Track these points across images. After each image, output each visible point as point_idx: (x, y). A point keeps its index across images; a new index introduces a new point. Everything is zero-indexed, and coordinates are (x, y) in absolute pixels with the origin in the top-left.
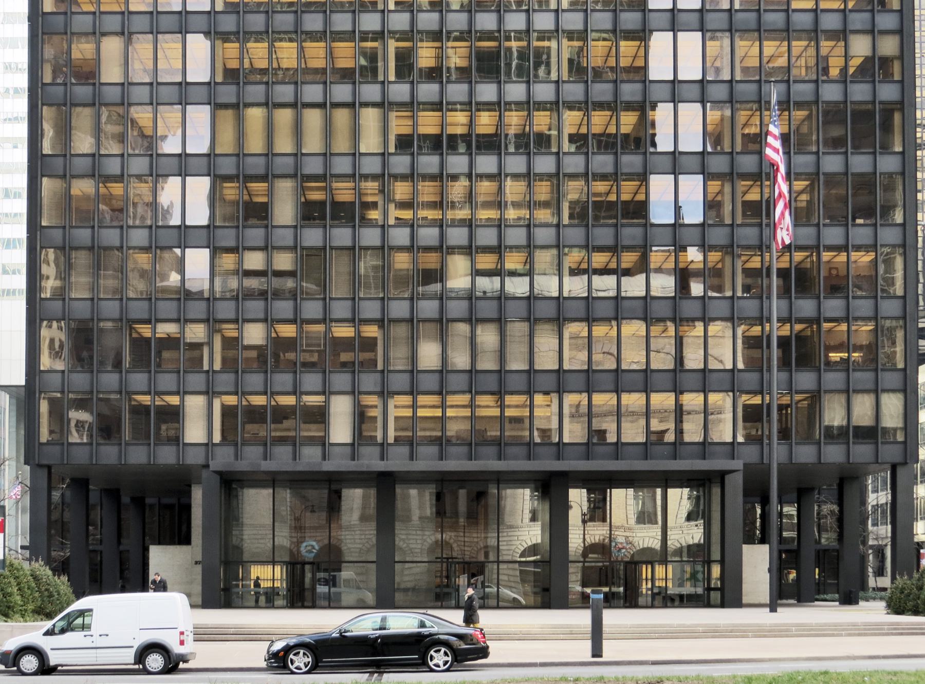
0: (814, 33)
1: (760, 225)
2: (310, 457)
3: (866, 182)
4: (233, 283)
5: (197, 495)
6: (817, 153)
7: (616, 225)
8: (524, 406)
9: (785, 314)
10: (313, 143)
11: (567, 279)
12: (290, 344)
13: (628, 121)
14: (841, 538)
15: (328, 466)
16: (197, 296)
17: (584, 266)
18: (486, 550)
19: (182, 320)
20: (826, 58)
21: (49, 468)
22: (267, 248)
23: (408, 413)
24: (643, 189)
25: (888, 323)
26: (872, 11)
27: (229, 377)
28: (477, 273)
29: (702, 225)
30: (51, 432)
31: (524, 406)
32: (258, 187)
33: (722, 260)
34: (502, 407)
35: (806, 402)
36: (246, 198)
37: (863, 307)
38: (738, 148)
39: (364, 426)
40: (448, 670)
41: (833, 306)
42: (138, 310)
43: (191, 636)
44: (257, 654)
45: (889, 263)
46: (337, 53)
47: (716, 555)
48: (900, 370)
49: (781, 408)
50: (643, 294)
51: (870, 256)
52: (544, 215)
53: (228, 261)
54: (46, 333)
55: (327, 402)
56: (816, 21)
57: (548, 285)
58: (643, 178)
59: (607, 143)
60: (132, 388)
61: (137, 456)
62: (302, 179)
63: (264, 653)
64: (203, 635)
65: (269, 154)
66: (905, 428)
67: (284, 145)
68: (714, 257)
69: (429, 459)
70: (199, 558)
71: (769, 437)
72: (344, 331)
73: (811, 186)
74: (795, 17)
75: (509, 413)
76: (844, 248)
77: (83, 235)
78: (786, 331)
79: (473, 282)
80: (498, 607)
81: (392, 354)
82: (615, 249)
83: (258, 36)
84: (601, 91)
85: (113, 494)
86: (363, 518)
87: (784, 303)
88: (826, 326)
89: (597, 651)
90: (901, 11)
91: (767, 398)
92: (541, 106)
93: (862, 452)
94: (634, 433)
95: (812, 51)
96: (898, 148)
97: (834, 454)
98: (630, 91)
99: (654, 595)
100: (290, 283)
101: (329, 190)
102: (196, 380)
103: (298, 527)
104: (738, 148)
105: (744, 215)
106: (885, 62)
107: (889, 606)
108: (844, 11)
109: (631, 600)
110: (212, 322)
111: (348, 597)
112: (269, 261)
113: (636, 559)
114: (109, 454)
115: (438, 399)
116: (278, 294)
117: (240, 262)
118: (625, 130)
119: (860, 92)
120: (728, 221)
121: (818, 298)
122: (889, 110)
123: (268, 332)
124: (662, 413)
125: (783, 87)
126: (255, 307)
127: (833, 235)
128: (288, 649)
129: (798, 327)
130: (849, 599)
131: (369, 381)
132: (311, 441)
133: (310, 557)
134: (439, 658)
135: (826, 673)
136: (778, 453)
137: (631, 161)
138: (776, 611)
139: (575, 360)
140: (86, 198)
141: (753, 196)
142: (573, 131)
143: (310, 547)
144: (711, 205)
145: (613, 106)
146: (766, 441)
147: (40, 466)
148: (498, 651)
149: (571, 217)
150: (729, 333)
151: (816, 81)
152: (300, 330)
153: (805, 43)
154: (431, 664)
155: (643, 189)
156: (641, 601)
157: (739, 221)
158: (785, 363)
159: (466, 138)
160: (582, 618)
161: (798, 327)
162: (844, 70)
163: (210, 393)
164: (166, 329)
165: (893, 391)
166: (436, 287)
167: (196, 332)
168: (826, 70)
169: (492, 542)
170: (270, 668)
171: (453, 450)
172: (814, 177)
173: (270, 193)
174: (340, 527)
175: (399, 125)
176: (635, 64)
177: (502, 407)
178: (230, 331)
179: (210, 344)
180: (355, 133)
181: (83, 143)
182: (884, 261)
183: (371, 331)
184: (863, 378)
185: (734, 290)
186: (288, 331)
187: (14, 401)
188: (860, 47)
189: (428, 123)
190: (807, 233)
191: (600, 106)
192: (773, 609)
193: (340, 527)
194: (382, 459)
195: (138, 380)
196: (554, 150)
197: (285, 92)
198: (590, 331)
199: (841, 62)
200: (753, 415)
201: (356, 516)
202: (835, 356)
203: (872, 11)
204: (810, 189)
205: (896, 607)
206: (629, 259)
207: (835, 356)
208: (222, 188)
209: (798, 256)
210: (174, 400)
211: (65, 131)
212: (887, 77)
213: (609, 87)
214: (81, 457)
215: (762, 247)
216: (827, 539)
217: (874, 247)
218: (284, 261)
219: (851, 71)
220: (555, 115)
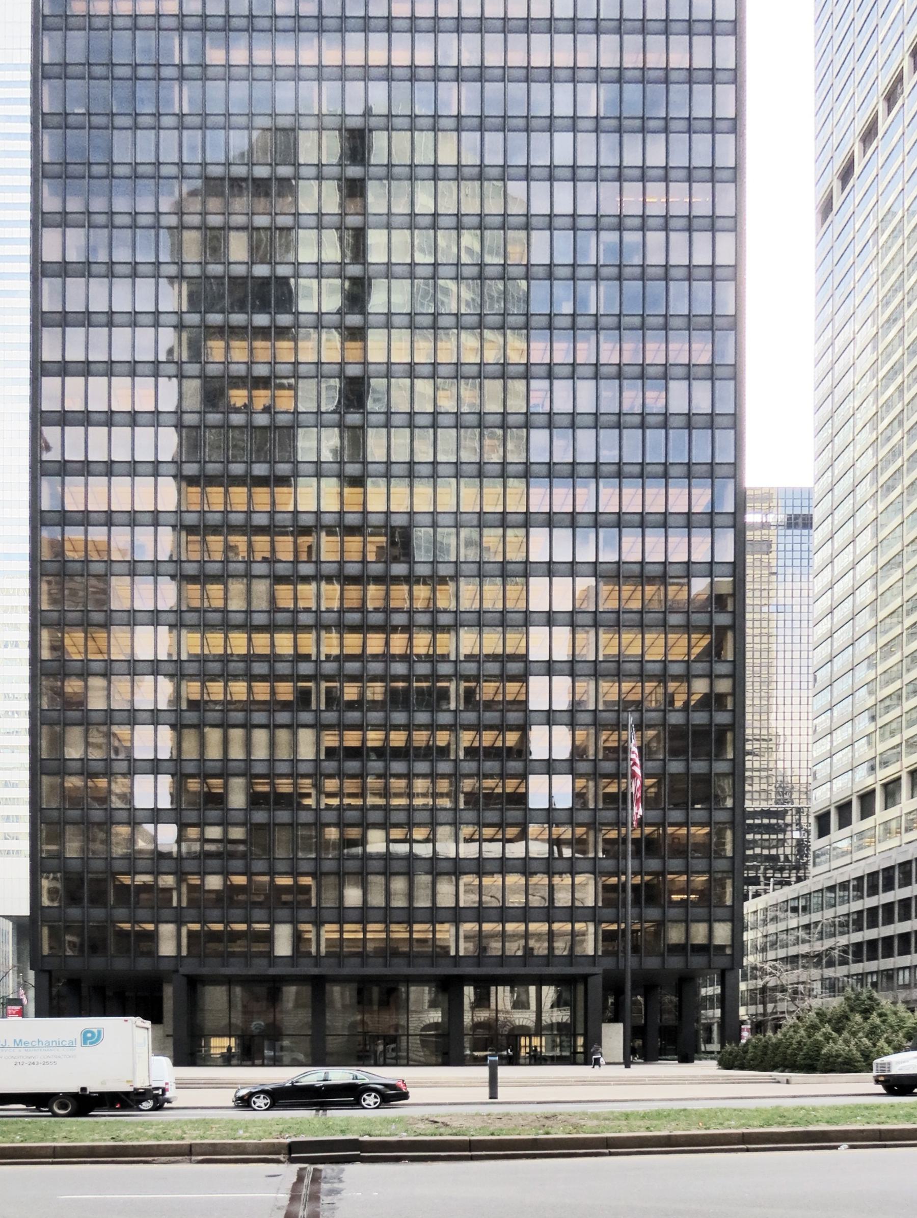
0: (663, 677)
1: (618, 809)
2: (259, 967)
3: (706, 779)
4: (196, 847)
5: (168, 991)
6: (664, 760)
7: (502, 711)
9: (637, 869)
10: (260, 752)
11: (462, 845)
12: (241, 889)
13: (512, 738)
14: (680, 1017)
15: (272, 971)
16: (167, 856)
17: (476, 837)
18: (397, 1027)
19: (156, 873)
20: (672, 695)
21: (50, 972)
22: (225, 823)
23: (336, 936)
24: (523, 785)
25: (719, 876)
26: (711, 662)
27: (193, 912)
28: (389, 841)
29: (571, 809)
30: (51, 948)
32: (216, 782)
33: (587, 833)
34: (365, 931)
36: (206, 789)
37: (700, 864)
38: (601, 756)
39: (301, 945)
40: (377, 1108)
41: (675, 864)
42: (118, 865)
43: (174, 1086)
44: (227, 1097)
45: (721, 834)
46: (255, 690)
47: (580, 1029)
49: (634, 932)
50: (523, 855)
51: (706, 830)
52: (446, 803)
53: (193, 832)
54: (45, 884)
55: (272, 928)
56: (665, 668)
57: (446, 849)
58: (524, 777)
59: (493, 753)
60: (116, 919)
61: (121, 964)
62: (249, 774)
63: (232, 1097)
64: (182, 1085)
65: (225, 760)
66: (732, 946)
67: (283, 753)
68: (580, 831)
69: (352, 968)
71: (624, 952)
72: (284, 881)
73: (659, 783)
74: (649, 666)
75: (415, 936)
76: (686, 824)
77: (74, 814)
78: (637, 880)
79: (388, 847)
80: (408, 1065)
81: (323, 896)
82: (501, 825)
83: (263, 678)
84: (491, 717)
86: (297, 1005)
87: (637, 862)
88: (670, 877)
89: (493, 1095)
90: (734, 661)
92: (443, 727)
93: (697, 961)
94: (515, 948)
95: (661, 690)
96: (730, 756)
97: (675, 963)
98: (514, 717)
99: (531, 1057)
100: (242, 848)
101: (273, 785)
102: (166, 913)
103: (247, 1012)
104: (601, 756)
105: (604, 802)
106: (721, 698)
107: (720, 1064)
108: (687, 661)
109: (513, 1061)
110: (180, 876)
111: (286, 1059)
112: (225, 832)
113: (516, 1032)
114: (98, 963)
115: (355, 737)
116: (232, 855)
117: (202, 833)
118: (508, 744)
119: (699, 718)
120: (591, 805)
121: (663, 858)
122: (722, 730)
123: (225, 881)
124: (539, 936)
125: (637, 715)
126: (214, 863)
127: (676, 815)
128: (251, 1095)
129: (647, 878)
130: (686, 1058)
131: (304, 914)
132: (261, 955)
133: (256, 1032)
134: (370, 1100)
135: (685, 1110)
136: (631, 962)
137: (514, 766)
139: (467, 900)
140: (76, 788)
141: (613, 789)
142: (467, 744)
143: (257, 1024)
144: (578, 796)
145: (502, 728)
146: (621, 954)
148: (415, 1095)
149: (466, 803)
150: (592, 882)
151: (664, 711)
152: (250, 880)
153: (655, 684)
154: (255, 1107)
155: (523, 785)
156: (522, 1061)
157: (601, 806)
158: (637, 902)
159: (428, 749)
160: (483, 1072)
161: (647, 878)
162: (687, 703)
163: (179, 922)
164: (141, 879)
165: (724, 921)
166: (359, 850)
167: (168, 881)
168: (672, 702)
169: (403, 1022)
170: (237, 1107)
171: (371, 960)
172: (661, 777)
173: (226, 786)
174: (281, 1012)
175: (330, 740)
176: (518, 698)
177: (411, 932)
178: (194, 880)
179: (179, 889)
180: (294, 745)
181: (74, 752)
182: (716, 834)
183: (306, 881)
184: (701, 912)
185: (596, 852)
186: (240, 880)
188: (700, 687)
189: (352, 739)
190: (654, 815)
191: (490, 728)
192: (627, 1066)
193: (281, 1012)
194: (316, 966)
195: (121, 912)
196: (452, 757)
197: (238, 717)
198: (480, 882)
199: (685, 697)
200: (609, 937)
201: (338, 1005)
202: (675, 897)
203: (711, 662)
204: (658, 785)
205: (726, 1064)
206: (511, 832)
207: (675, 897)
208: (186, 783)
209: (648, 830)
210: (150, 927)
211: (59, 742)
212: (721, 707)
213: (497, 714)
214: (76, 965)
215: (619, 823)
216: (669, 1019)
217: (708, 824)
218: (237, 833)
219: (692, 703)
220: (453, 735)
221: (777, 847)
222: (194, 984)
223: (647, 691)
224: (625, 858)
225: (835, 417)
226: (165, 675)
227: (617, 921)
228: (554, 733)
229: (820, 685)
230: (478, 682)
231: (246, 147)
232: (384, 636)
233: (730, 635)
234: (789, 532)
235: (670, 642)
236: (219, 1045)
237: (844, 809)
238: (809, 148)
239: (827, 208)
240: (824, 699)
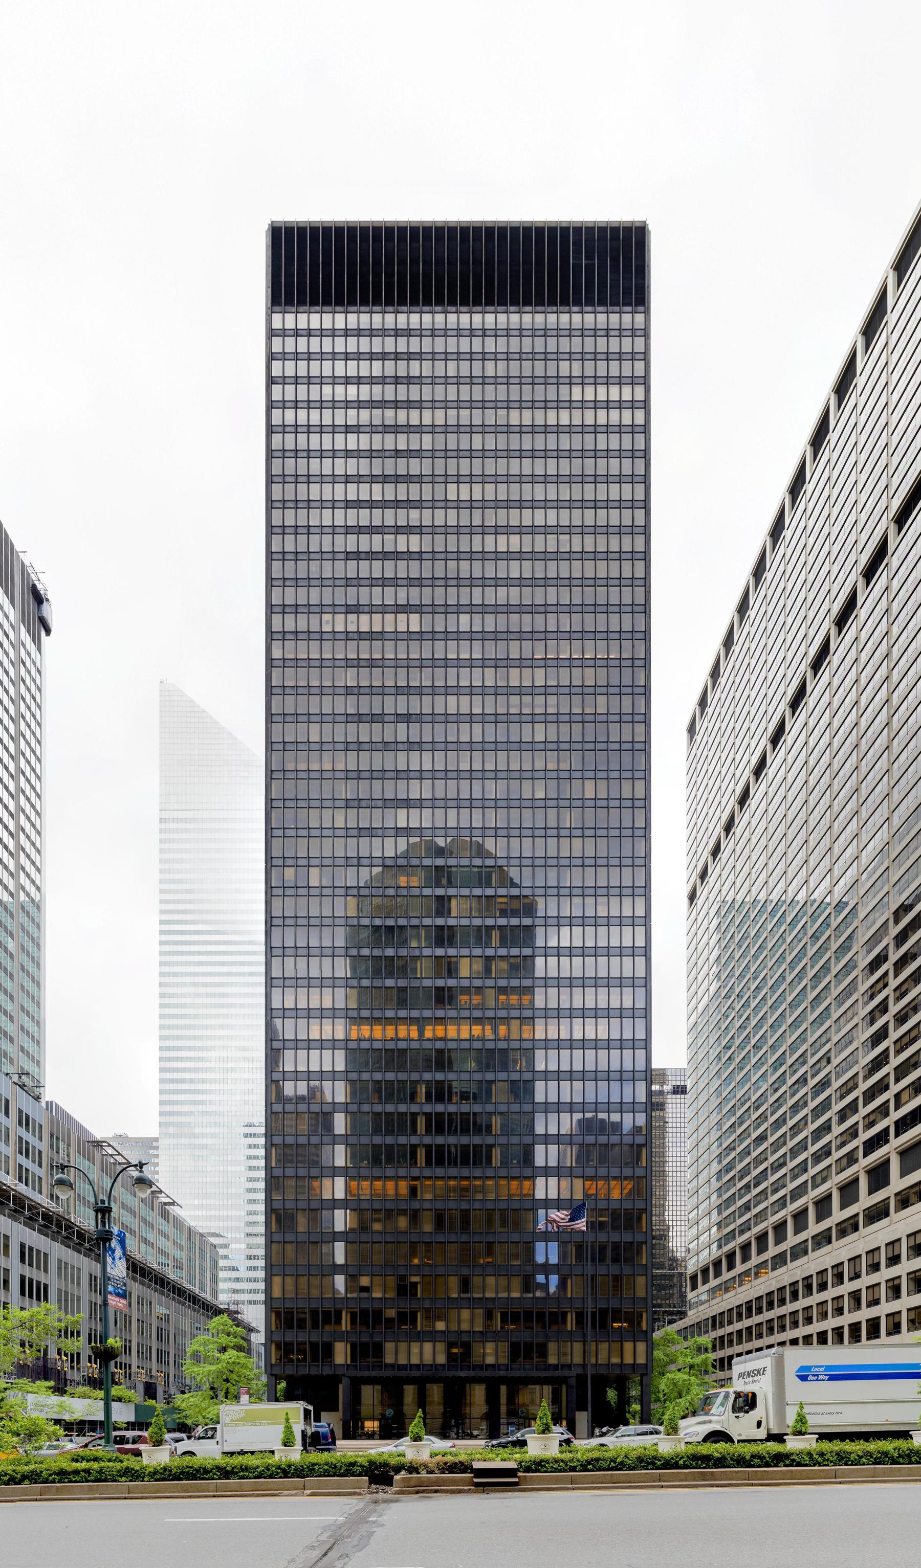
221: (668, 1299)
222: (356, 1384)
223: (599, 1186)
229: (692, 1223)
231: (369, 878)
233: (644, 1150)
234: (674, 1096)
235: (611, 1186)
236: (371, 1425)
237: (705, 1271)
238: (684, 861)
239: (692, 897)
240: (694, 1200)
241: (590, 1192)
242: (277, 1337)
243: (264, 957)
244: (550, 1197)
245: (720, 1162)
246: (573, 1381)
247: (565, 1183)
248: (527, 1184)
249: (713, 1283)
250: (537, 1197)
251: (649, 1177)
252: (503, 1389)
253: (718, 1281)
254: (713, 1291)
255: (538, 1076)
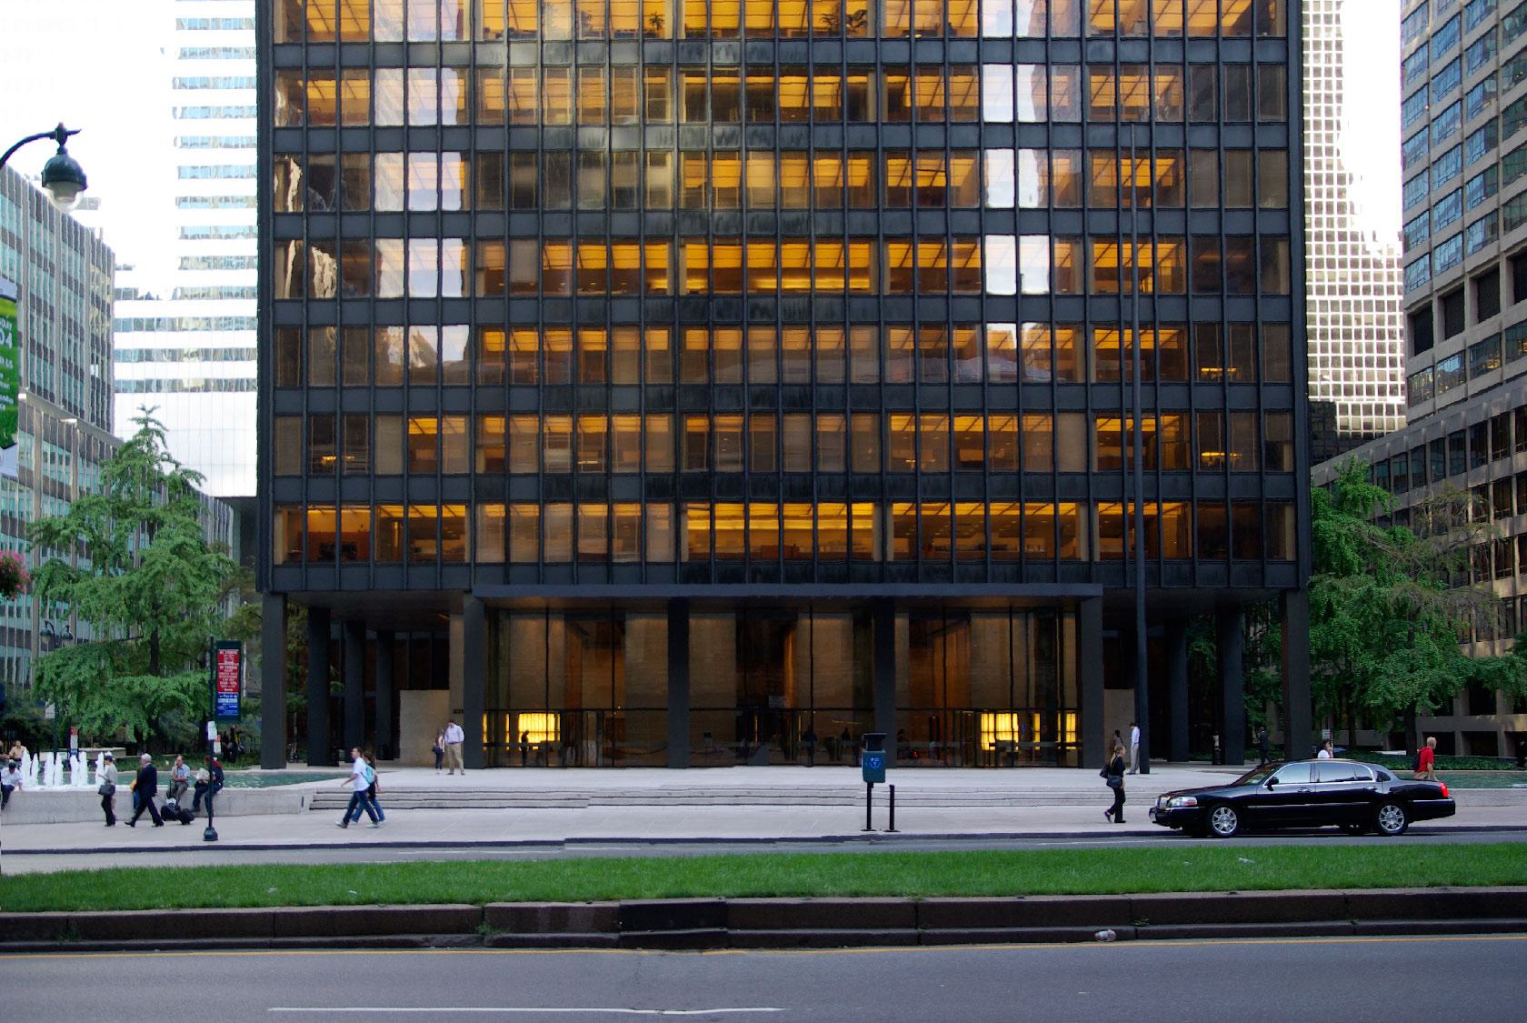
5: (457, 628)
8: (838, 517)
9: (1147, 317)
21: (285, 596)
31: (838, 517)
34: (815, 518)
35: (1175, 513)
38: (1093, 379)
48: (1290, 563)
70: (460, 705)
85: (356, 625)
91: (1129, 423)
138: (1148, 772)
147: (274, 593)
187: (239, 516)
196: (872, 119)
224: (1132, 473)
225: (1435, 173)
226: (452, 67)
227: (1120, 500)
228: (1022, 246)
230: (908, 74)
232: (773, 246)
236: (537, 727)
241: (1132, 102)
242: (366, 260)
243: (254, 122)
244: (1023, 204)
245: (1491, 143)
246: (1094, 613)
247: (1062, 81)
248: (959, 83)
249: (1474, 332)
250: (988, 117)
251: (1295, 235)
252: (901, 623)
253: (1489, 328)
254: (1479, 349)
255: (988, 50)
